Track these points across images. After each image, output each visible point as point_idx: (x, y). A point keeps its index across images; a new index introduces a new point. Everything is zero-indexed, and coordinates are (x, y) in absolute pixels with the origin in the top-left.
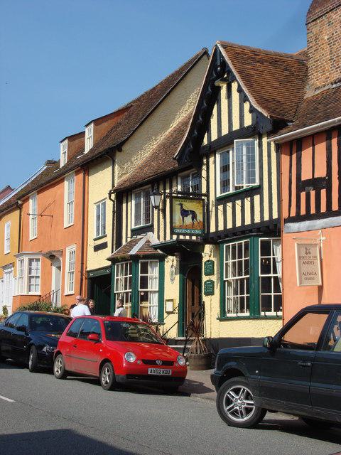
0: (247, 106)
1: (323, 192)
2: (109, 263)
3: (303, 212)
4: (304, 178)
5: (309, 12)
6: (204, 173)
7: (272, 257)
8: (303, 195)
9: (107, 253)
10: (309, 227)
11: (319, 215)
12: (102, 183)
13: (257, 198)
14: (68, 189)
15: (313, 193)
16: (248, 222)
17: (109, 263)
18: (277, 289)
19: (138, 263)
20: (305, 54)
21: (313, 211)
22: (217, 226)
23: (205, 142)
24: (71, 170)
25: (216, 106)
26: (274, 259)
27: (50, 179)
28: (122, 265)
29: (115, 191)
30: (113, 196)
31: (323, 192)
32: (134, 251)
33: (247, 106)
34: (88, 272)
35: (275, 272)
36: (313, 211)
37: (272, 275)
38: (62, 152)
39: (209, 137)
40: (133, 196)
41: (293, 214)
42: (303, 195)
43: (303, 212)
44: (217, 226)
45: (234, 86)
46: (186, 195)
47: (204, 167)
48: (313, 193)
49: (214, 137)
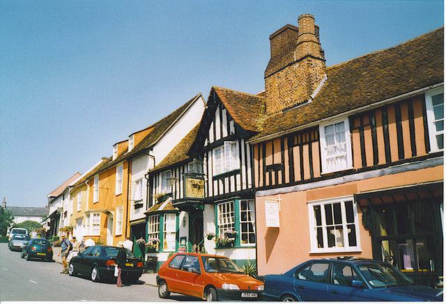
0: (232, 123)
1: (280, 172)
2: (145, 216)
3: (267, 184)
4: (239, 175)
5: (268, 68)
6: (205, 162)
7: (247, 211)
8: (267, 174)
9: (143, 210)
10: (365, 176)
11: (277, 186)
12: (140, 173)
13: (238, 176)
14: (120, 176)
15: (273, 173)
16: (221, 193)
17: (145, 216)
18: (251, 230)
19: (155, 216)
20: (263, 94)
21: (280, 182)
22: (236, 189)
23: (206, 144)
24: (121, 161)
25: (212, 123)
26: (249, 212)
27: (107, 169)
28: (224, 206)
29: (148, 173)
30: (147, 176)
31: (280, 172)
32: (160, 209)
33: (232, 123)
34: (130, 222)
35: (250, 220)
36: (274, 183)
37: (248, 221)
38: (114, 152)
39: (208, 140)
40: (214, 151)
41: (261, 185)
42: (267, 174)
43: (267, 184)
44: (236, 189)
45: (224, 112)
46: (193, 175)
47: (205, 159)
48: (273, 173)
49: (212, 141)
